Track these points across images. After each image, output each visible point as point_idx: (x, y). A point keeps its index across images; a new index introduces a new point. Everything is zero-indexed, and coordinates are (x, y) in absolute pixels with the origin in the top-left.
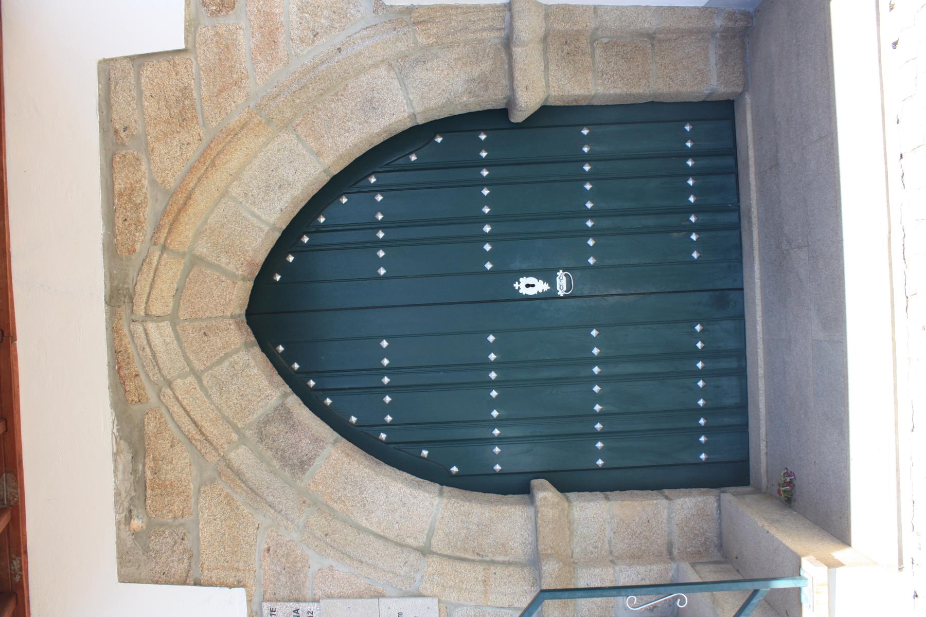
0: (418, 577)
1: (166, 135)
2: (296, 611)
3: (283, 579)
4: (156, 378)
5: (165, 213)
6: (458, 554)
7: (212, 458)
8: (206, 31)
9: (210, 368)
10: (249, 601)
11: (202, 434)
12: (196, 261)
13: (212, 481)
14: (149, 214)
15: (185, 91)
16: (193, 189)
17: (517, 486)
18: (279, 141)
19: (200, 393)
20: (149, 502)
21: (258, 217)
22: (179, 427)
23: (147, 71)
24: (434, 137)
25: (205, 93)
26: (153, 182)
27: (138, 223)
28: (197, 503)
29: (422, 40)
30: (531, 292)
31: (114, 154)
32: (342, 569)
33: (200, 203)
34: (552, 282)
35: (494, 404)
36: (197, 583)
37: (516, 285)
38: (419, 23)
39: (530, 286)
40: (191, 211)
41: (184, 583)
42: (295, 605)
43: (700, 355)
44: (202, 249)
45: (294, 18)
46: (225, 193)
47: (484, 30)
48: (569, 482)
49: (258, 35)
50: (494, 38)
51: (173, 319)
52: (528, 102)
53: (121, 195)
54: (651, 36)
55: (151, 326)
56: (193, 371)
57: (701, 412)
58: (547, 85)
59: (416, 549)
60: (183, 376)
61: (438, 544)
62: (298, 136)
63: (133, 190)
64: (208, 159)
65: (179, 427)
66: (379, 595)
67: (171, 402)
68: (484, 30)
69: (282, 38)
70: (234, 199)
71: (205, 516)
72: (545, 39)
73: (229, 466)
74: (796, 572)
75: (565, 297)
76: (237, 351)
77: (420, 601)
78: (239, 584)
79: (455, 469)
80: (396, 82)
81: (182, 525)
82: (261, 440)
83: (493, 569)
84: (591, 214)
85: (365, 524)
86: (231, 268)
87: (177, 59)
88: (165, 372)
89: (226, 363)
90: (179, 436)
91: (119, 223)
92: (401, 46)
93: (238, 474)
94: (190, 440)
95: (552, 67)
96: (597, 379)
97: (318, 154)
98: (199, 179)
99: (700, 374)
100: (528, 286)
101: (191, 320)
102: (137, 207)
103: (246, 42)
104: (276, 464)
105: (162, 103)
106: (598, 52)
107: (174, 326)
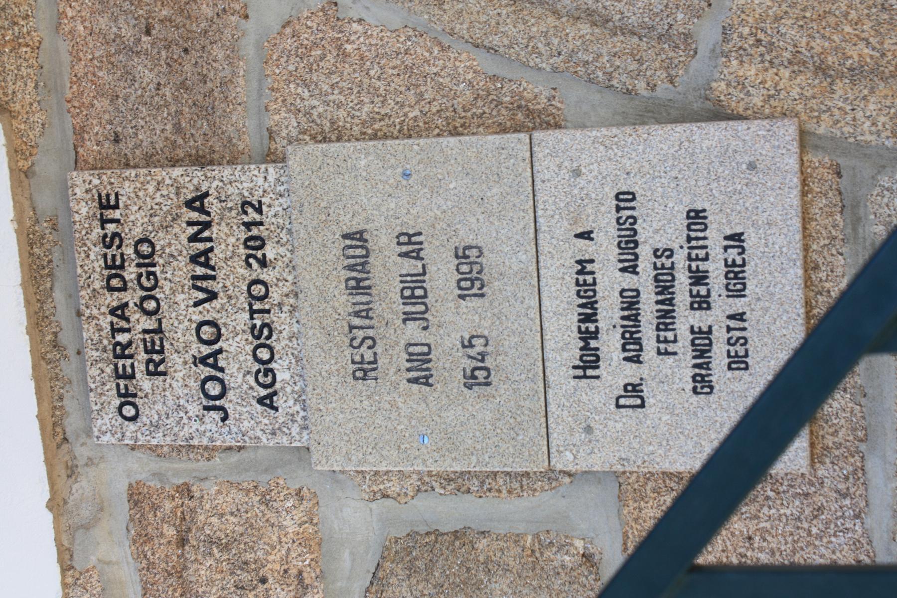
0: (708, 34)
2: (197, 202)
3: (146, 75)
42: (192, 179)
66: (533, 119)
77: (714, 133)
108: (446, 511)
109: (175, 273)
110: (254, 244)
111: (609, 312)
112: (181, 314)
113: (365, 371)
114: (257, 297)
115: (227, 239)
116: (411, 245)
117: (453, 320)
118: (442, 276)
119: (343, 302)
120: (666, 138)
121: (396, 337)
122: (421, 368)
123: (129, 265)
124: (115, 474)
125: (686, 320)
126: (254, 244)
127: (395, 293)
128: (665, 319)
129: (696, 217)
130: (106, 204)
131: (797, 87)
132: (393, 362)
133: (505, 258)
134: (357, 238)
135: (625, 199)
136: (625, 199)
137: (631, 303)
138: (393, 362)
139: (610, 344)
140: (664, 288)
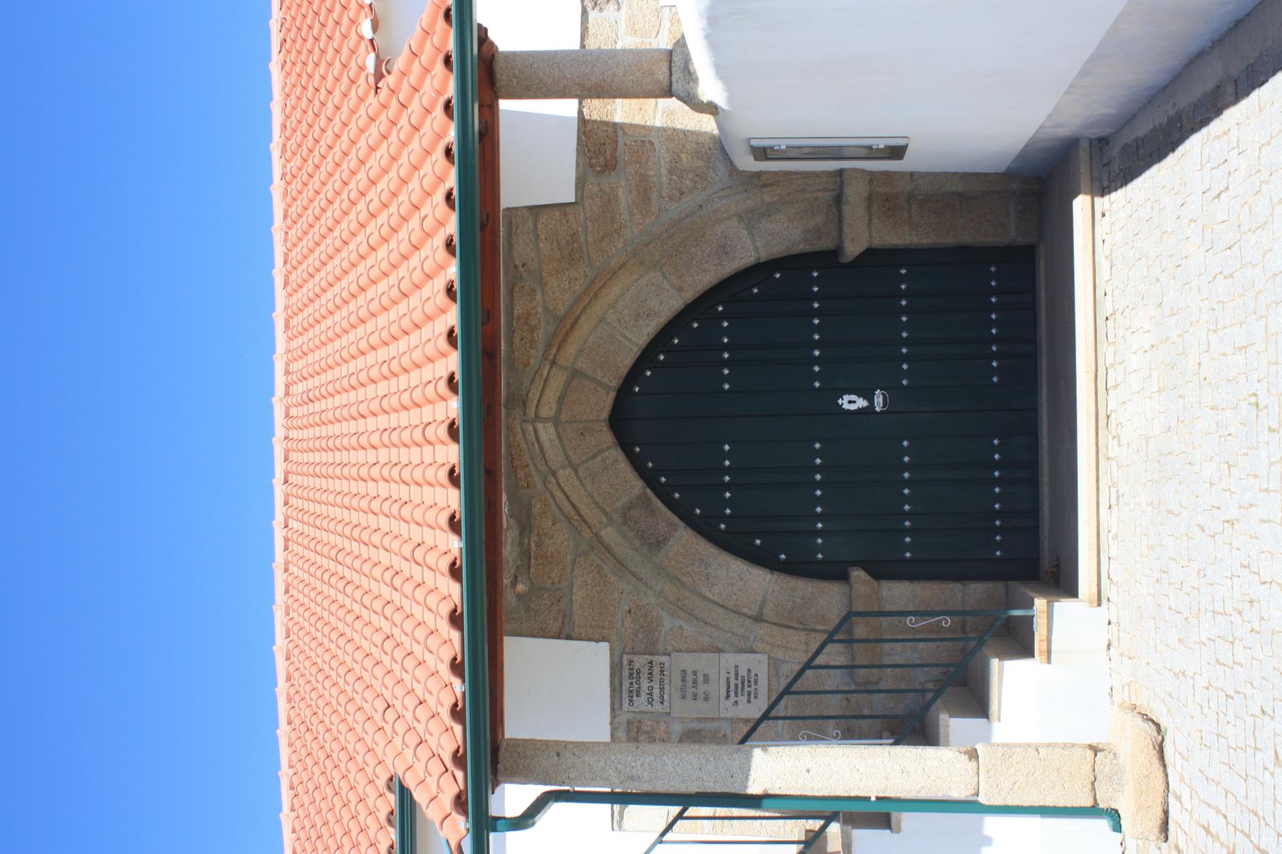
0: (752, 637)
1: (557, 271)
2: (651, 662)
3: (640, 636)
4: (543, 468)
5: (555, 334)
6: (785, 623)
7: (587, 534)
8: (592, 188)
9: (587, 460)
10: (612, 654)
11: (579, 514)
12: (575, 374)
13: (586, 554)
14: (541, 335)
15: (574, 236)
16: (579, 316)
17: (836, 572)
18: (647, 277)
19: (577, 483)
20: (532, 570)
21: (630, 340)
22: (560, 509)
23: (543, 218)
24: (774, 273)
25: (590, 239)
26: (546, 309)
27: (533, 342)
28: (572, 571)
29: (767, 198)
30: (853, 407)
31: (514, 285)
32: (689, 629)
33: (585, 325)
34: (870, 400)
35: (818, 501)
36: (569, 638)
37: (840, 401)
38: (766, 186)
39: (852, 403)
40: (576, 333)
41: (558, 637)
42: (649, 658)
43: (997, 465)
44: (582, 364)
45: (664, 179)
46: (602, 319)
47: (819, 191)
48: (882, 571)
49: (635, 193)
50: (828, 196)
51: (556, 421)
52: (853, 249)
53: (519, 319)
54: (960, 195)
55: (540, 426)
56: (571, 464)
57: (997, 514)
58: (870, 236)
59: (750, 617)
60: (564, 468)
61: (768, 613)
62: (664, 274)
63: (529, 314)
64: (592, 292)
65: (560, 509)
66: (720, 651)
67: (554, 488)
68: (819, 191)
69: (654, 195)
70: (610, 324)
71: (578, 582)
72: (869, 198)
73: (600, 541)
74: (1030, 605)
75: (882, 412)
76: (608, 449)
77: (752, 656)
78: (604, 639)
79: (783, 556)
80: (745, 232)
81: (559, 589)
82: (625, 523)
83: (813, 635)
84: (905, 342)
85: (709, 595)
86: (605, 380)
87: (568, 210)
88: (550, 463)
89: (599, 458)
90: (558, 515)
91: (517, 341)
92: (751, 204)
93: (608, 548)
94: (569, 519)
95: (875, 220)
96: (907, 483)
97: (680, 290)
98: (584, 309)
99: (997, 482)
100: (850, 402)
101: (570, 422)
102: (532, 329)
103: (624, 198)
104: (637, 543)
105: (555, 245)
106: (914, 208)
107: (556, 426)
108: (696, 725)
109: (644, 676)
110: (662, 671)
111: (732, 687)
112: (645, 684)
113: (684, 697)
114: (662, 681)
115: (656, 670)
116: (695, 673)
117: (702, 688)
118: (701, 679)
119: (680, 683)
120: (744, 656)
121: (690, 691)
122: (695, 697)
123: (635, 675)
124: (623, 718)
125: (746, 689)
126: (662, 671)
127: (690, 684)
128: (743, 689)
129: (749, 671)
130: (630, 662)
131: (767, 648)
132: (689, 695)
133: (713, 676)
134: (684, 671)
135: (736, 667)
136: (736, 667)
137: (736, 686)
138: (689, 695)
139: (732, 693)
140: (743, 683)
